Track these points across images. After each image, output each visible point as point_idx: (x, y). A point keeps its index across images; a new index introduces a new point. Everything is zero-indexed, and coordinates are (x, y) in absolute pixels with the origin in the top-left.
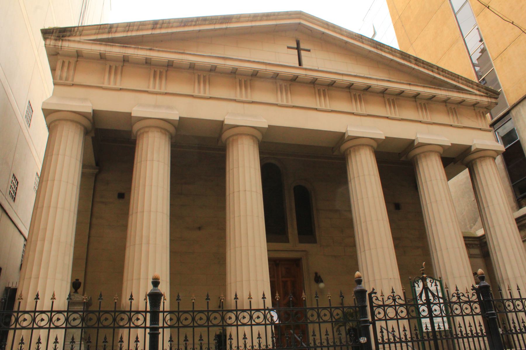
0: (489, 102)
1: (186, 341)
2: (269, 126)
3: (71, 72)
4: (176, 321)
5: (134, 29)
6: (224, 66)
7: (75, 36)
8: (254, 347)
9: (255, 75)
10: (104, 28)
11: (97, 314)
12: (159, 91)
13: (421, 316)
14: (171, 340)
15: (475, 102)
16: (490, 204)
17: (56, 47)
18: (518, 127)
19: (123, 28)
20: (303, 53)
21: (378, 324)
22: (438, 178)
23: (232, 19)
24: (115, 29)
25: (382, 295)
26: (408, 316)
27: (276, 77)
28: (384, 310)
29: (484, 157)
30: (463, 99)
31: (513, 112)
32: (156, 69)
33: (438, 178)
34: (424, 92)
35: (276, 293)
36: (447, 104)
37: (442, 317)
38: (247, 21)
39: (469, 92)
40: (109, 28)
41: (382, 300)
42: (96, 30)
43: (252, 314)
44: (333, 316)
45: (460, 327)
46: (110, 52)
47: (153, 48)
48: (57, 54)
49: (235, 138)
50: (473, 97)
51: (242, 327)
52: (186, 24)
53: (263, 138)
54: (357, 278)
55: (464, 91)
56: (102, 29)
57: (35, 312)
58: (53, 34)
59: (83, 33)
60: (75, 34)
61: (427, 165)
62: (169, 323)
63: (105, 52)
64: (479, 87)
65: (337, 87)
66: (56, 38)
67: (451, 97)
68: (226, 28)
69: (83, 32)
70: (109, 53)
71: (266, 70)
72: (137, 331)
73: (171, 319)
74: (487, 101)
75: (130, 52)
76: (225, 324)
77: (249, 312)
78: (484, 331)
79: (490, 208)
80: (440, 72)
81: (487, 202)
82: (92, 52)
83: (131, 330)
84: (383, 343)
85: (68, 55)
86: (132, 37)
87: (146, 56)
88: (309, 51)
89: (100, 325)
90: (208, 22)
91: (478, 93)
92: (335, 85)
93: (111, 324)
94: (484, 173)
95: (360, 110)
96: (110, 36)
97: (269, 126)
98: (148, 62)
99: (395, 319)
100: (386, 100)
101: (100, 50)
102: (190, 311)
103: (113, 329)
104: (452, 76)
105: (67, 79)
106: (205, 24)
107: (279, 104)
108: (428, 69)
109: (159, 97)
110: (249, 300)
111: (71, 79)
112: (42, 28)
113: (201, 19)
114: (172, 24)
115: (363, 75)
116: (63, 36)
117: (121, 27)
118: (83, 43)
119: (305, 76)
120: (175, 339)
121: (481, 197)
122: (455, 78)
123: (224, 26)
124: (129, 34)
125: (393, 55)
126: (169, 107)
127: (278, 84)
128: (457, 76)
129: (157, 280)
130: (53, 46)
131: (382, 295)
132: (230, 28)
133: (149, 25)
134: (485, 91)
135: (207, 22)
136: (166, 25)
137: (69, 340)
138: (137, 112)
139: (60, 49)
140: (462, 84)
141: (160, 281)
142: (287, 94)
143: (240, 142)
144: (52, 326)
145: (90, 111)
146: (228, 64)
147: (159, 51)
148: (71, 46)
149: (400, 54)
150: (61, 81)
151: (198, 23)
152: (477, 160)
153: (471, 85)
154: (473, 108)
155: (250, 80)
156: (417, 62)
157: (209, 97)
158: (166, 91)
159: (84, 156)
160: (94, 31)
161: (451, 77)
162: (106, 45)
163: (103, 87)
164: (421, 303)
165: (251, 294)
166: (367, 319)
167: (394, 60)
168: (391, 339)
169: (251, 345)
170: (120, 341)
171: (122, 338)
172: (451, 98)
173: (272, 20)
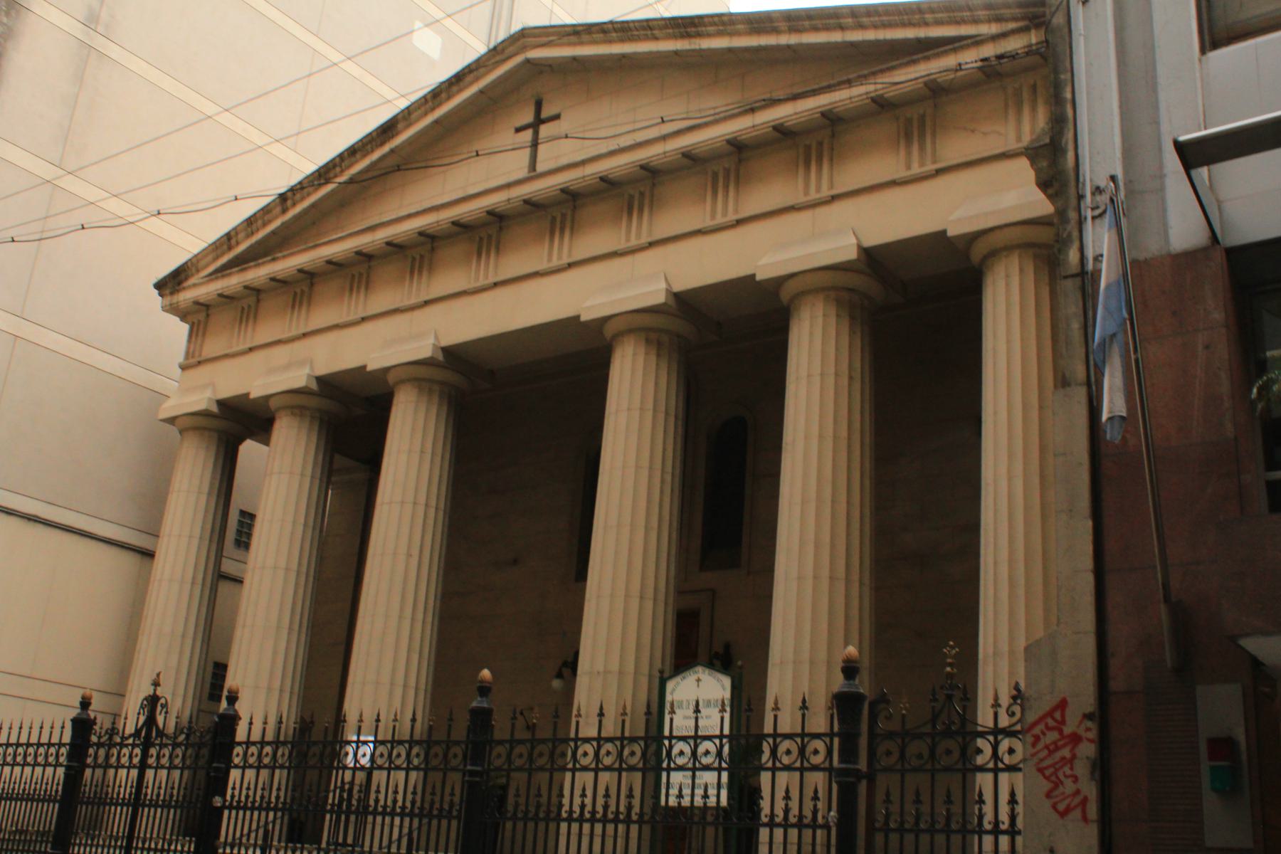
7: (192, 275)
12: (818, 196)
37: (720, 770)
39: (950, 47)
50: (970, 58)
57: (803, 735)
78: (60, 793)
84: (887, 830)
88: (557, 117)
106: (357, 162)
111: (197, 354)
112: (155, 281)
119: (752, 129)
123: (386, 148)
129: (854, 665)
131: (101, 728)
135: (358, 156)
140: (939, 23)
141: (239, 695)
145: (852, 254)
149: (748, 23)
153: (968, 14)
157: (360, 320)
158: (649, 240)
162: (223, 276)
163: (703, 230)
165: (381, 715)
166: (1213, 763)
171: (981, 794)
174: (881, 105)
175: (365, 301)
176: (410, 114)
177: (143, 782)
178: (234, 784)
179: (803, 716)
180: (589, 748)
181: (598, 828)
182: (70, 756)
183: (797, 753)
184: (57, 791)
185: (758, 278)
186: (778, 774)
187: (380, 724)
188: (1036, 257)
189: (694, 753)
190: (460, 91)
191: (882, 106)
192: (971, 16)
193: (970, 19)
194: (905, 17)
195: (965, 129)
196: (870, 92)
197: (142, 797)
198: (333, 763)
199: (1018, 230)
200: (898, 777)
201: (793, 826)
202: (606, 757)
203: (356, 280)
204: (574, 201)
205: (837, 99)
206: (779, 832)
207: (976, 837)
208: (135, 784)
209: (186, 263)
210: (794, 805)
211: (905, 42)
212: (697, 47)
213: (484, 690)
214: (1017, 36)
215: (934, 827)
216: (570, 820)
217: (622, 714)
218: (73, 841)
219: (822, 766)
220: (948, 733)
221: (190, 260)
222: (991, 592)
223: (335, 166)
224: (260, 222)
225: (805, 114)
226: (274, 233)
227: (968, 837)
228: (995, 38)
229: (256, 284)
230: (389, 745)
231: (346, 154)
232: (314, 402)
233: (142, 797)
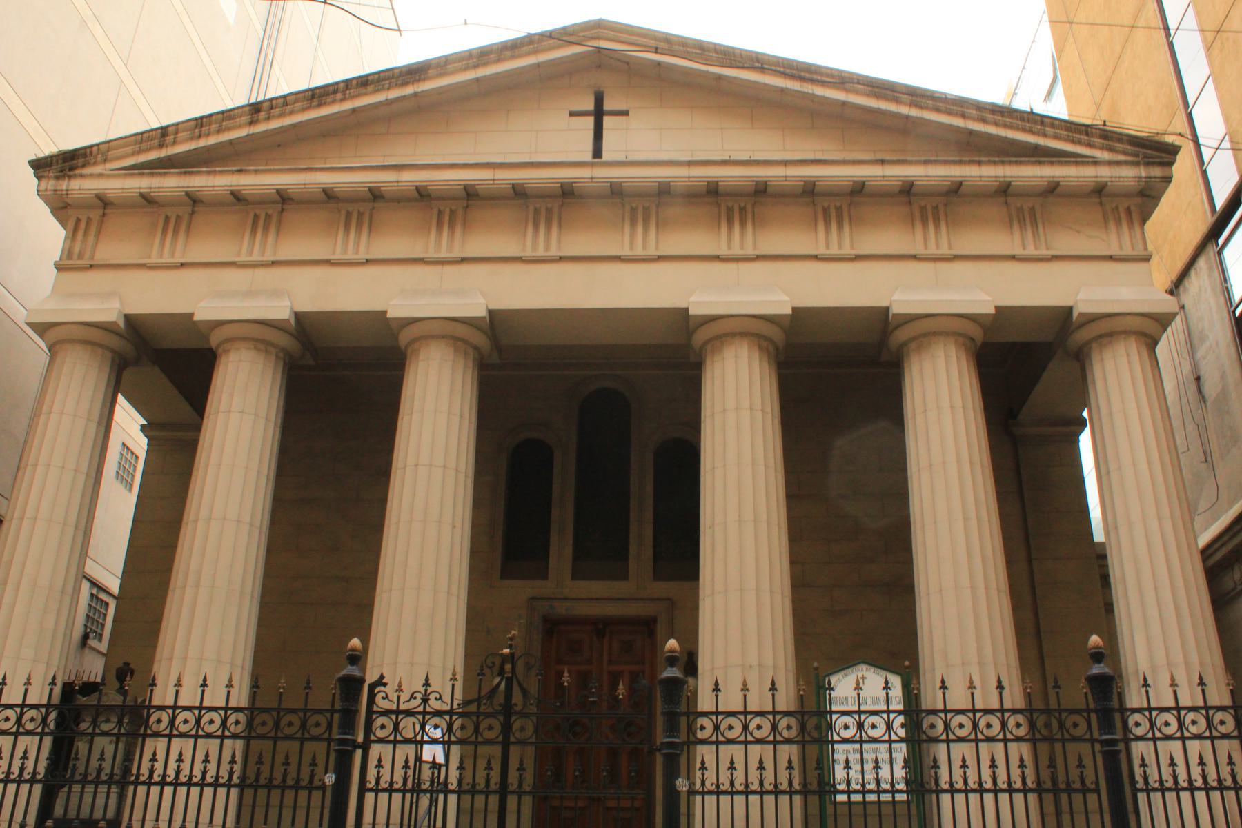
0: (1140, 177)
1: (936, 769)
3: (91, 239)
4: (769, 732)
5: (212, 130)
6: (398, 186)
7: (95, 163)
8: (721, 786)
9: (470, 194)
10: (150, 138)
11: (301, 714)
12: (260, 259)
13: (1132, 736)
14: (461, 767)
15: (1093, 184)
17: (58, 193)
19: (189, 133)
20: (608, 121)
21: (514, 752)
23: (428, 69)
24: (172, 137)
25: (400, 690)
27: (519, 193)
28: (1207, 718)
29: (1110, 336)
30: (1051, 179)
32: (258, 212)
33: (945, 403)
34: (927, 176)
35: (126, 677)
36: (1104, 199)
38: (466, 69)
39: (1073, 159)
40: (159, 136)
41: (395, 700)
42: (135, 144)
43: (1006, 718)
44: (1065, 726)
46: (159, 188)
47: (244, 168)
48: (66, 206)
50: (1088, 172)
52: (323, 102)
53: (985, 335)
54: (1091, 649)
55: (1055, 159)
56: (146, 142)
57: (200, 708)
58: (53, 167)
59: (109, 157)
60: (93, 161)
62: (458, 733)
63: (149, 190)
64: (1112, 141)
66: (58, 174)
67: (1014, 179)
68: (415, 95)
69: (109, 153)
70: (157, 190)
71: (786, 177)
73: (463, 727)
74: (1133, 177)
75: (203, 182)
76: (692, 739)
77: (971, 715)
80: (984, 114)
82: (126, 193)
83: (199, 740)
85: (83, 205)
86: (208, 149)
87: (231, 186)
88: (625, 113)
89: (306, 735)
90: (372, 86)
92: (962, 189)
93: (270, 731)
95: (339, 250)
96: (163, 153)
98: (238, 198)
101: (140, 188)
102: (271, 709)
103: (299, 742)
104: (1022, 120)
105: (81, 256)
106: (366, 94)
107: (919, 255)
109: (260, 273)
110: (970, 690)
111: (87, 255)
114: (292, 106)
115: (745, 157)
116: (71, 169)
117: (183, 132)
118: (108, 176)
120: (469, 764)
122: (1033, 125)
123: (409, 90)
124: (203, 143)
127: (723, 208)
128: (1039, 118)
130: (53, 193)
131: (400, 690)
132: (423, 91)
133: (241, 116)
134: (1129, 147)
135: (370, 88)
136: (278, 110)
137: (253, 759)
138: (398, 309)
139: (65, 196)
140: (1056, 137)
143: (422, 355)
144: (201, 733)
145: (482, 312)
146: (404, 179)
147: (256, 172)
148: (85, 188)
150: (70, 262)
151: (350, 93)
152: (1094, 345)
153: (1086, 138)
154: (1097, 200)
155: (753, 206)
156: (914, 98)
158: (272, 259)
160: (130, 149)
161: (1019, 122)
162: (152, 174)
167: (849, 103)
169: (978, 780)
170: (933, 767)
171: (935, 760)
173: (528, 54)
174: (1004, 191)
175: (185, 246)
177: (71, 750)
179: (773, 695)
180: (295, 719)
181: (155, 790)
182: (60, 722)
185: (196, 318)
186: (981, 745)
188: (956, 342)
189: (198, 722)
191: (421, 195)
192: (1088, 140)
193: (1086, 141)
194: (1027, 124)
195: (1070, 228)
196: (999, 177)
198: (139, 730)
199: (1138, 320)
200: (298, 744)
201: (209, 785)
202: (487, 730)
203: (447, 218)
204: (193, 206)
205: (968, 174)
206: (960, 798)
207: (934, 796)
209: (91, 146)
210: (292, 769)
211: (1013, 142)
212: (811, 92)
214: (1129, 167)
215: (299, 783)
216: (952, 791)
217: (969, 688)
219: (796, 739)
221: (98, 145)
223: (335, 92)
224: (214, 127)
225: (936, 179)
226: (231, 142)
227: (927, 797)
228: (1110, 163)
229: (111, 195)
230: (43, 710)
231: (354, 82)
232: (114, 342)
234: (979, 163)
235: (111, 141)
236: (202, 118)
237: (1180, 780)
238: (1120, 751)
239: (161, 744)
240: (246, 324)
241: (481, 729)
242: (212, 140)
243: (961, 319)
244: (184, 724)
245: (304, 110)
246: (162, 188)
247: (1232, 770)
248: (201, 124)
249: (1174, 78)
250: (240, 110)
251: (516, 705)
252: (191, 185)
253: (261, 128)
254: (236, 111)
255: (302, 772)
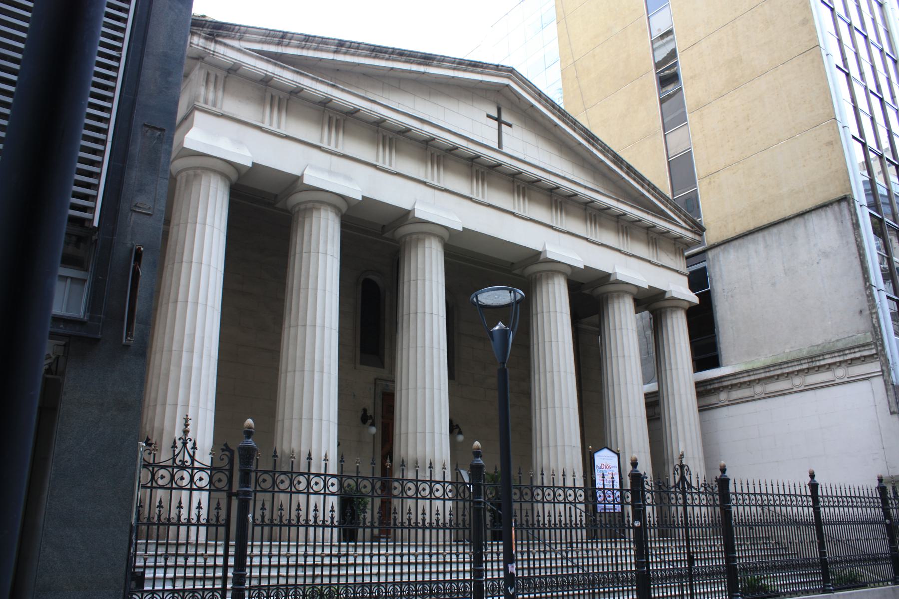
2: (253, 164)
16: (673, 367)
18: (713, 274)
22: (630, 328)
26: (373, 493)
29: (677, 308)
31: (710, 254)
36: (649, 232)
45: (409, 513)
49: (420, 236)
51: (178, 491)
61: (620, 308)
63: (273, 75)
65: (411, 139)
70: (278, 77)
72: (181, 494)
79: (674, 371)
81: (670, 364)
85: (217, 66)
87: (326, 94)
88: (510, 126)
90: (405, 58)
91: (683, 224)
94: (673, 328)
97: (253, 164)
99: (441, 499)
100: (516, 186)
106: (399, 61)
108: (638, 182)
113: (397, 51)
118: (245, 53)
121: (293, 274)
123: (422, 69)
124: (305, 53)
125: (605, 156)
126: (348, 178)
127: (677, 246)
136: (352, 50)
137: (214, 505)
140: (670, 209)
142: (483, 185)
152: (668, 310)
154: (674, 242)
159: (289, 244)
164: (679, 491)
168: (212, 520)
171: (395, 509)
172: (274, 79)
176: (443, 61)
178: (649, 514)
181: (302, 530)
183: (226, 481)
184: (812, 520)
187: (544, 476)
190: (472, 72)
197: (648, 523)
208: (720, 515)
213: (249, 434)
215: (308, 523)
218: (484, 559)
220: (183, 467)
221: (240, 26)
222: (443, 411)
233: (648, 523)
234: (648, 213)
235: (249, 27)
236: (309, 36)
237: (301, 519)
238: (250, 499)
239: (185, 494)
240: (440, 227)
241: (214, 481)
242: (311, 54)
243: (230, 166)
244: (200, 481)
245: (366, 56)
246: (282, 77)
247: (316, 514)
248: (307, 40)
249: (668, 179)
250: (332, 41)
251: (187, 462)
252: (301, 83)
253: (340, 58)
254: (330, 41)
255: (292, 515)
